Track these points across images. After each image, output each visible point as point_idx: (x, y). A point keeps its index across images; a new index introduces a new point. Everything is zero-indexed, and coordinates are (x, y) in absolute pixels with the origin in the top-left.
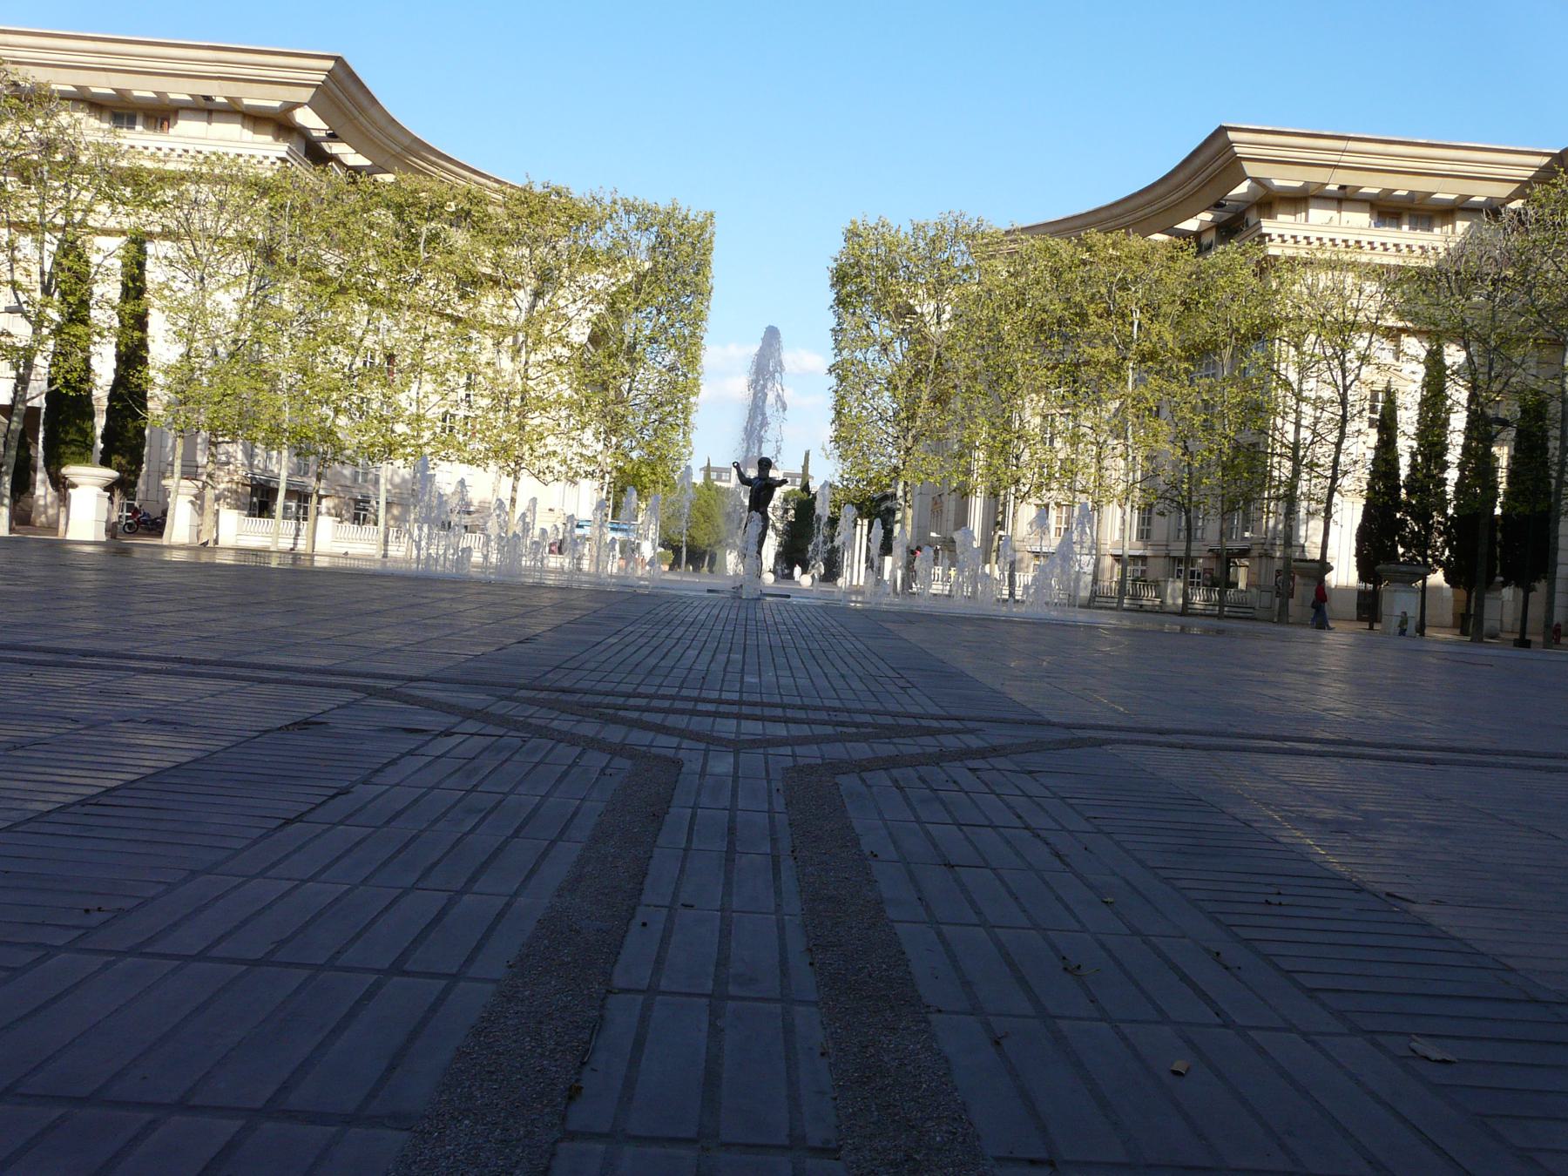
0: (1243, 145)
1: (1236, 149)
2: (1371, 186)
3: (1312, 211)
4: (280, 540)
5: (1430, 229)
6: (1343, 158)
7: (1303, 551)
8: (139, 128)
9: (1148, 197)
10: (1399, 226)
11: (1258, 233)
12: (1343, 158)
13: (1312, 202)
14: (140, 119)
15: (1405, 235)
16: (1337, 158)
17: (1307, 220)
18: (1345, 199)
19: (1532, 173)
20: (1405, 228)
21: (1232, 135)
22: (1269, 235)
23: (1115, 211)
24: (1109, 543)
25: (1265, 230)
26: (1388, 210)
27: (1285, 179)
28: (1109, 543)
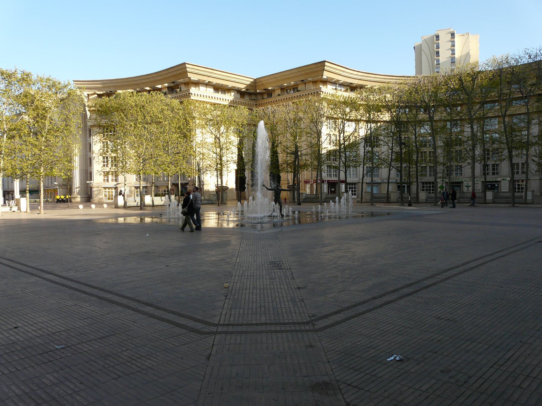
0: (189, 68)
1: (187, 69)
2: (215, 81)
3: (200, 87)
4: (515, 200)
5: (225, 94)
6: (212, 75)
7: (203, 182)
8: (220, 93)
9: (149, 77)
10: (218, 93)
11: (189, 92)
12: (212, 75)
13: (200, 85)
14: (220, 91)
15: (220, 95)
16: (210, 74)
17: (199, 90)
18: (208, 84)
19: (249, 83)
20: (220, 93)
21: (187, 65)
22: (191, 93)
23: (135, 79)
24: (133, 183)
25: (191, 92)
26: (218, 88)
27: (194, 78)
28: (133, 183)
